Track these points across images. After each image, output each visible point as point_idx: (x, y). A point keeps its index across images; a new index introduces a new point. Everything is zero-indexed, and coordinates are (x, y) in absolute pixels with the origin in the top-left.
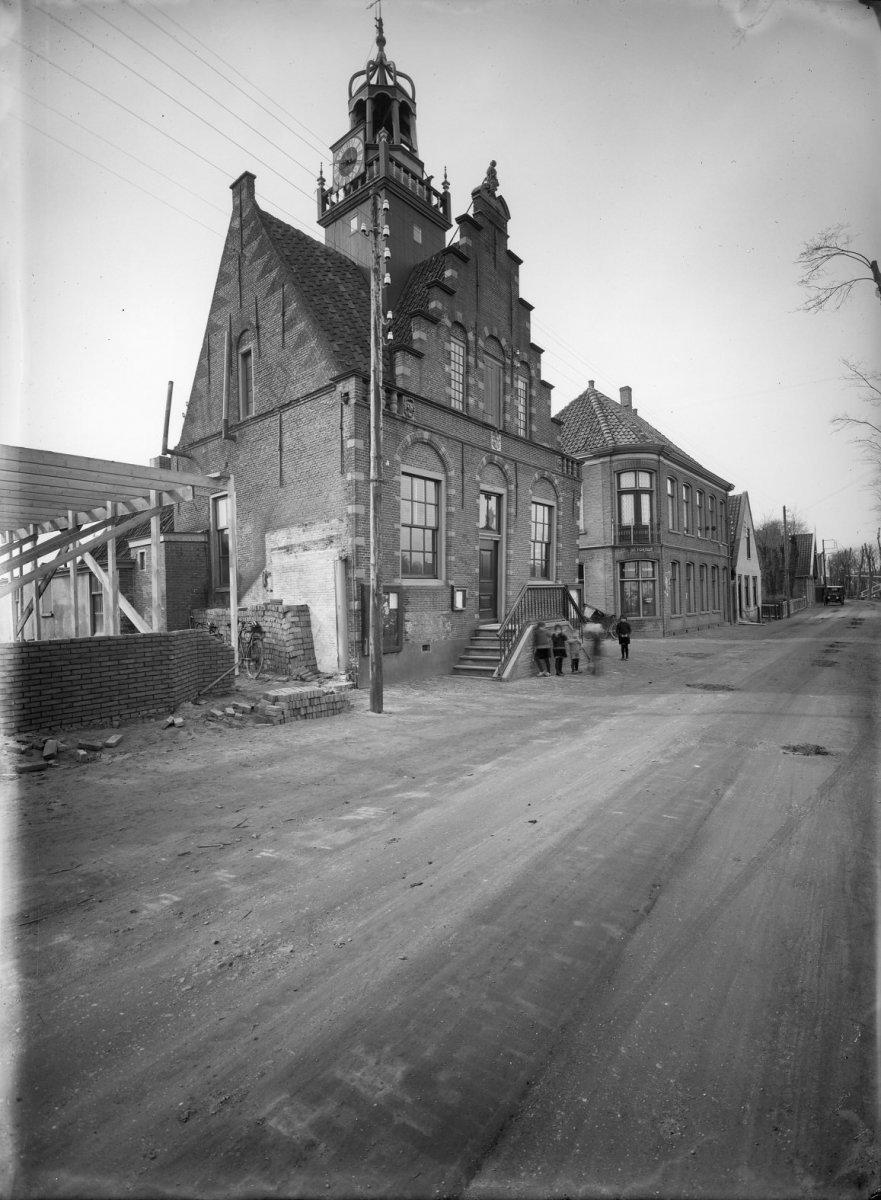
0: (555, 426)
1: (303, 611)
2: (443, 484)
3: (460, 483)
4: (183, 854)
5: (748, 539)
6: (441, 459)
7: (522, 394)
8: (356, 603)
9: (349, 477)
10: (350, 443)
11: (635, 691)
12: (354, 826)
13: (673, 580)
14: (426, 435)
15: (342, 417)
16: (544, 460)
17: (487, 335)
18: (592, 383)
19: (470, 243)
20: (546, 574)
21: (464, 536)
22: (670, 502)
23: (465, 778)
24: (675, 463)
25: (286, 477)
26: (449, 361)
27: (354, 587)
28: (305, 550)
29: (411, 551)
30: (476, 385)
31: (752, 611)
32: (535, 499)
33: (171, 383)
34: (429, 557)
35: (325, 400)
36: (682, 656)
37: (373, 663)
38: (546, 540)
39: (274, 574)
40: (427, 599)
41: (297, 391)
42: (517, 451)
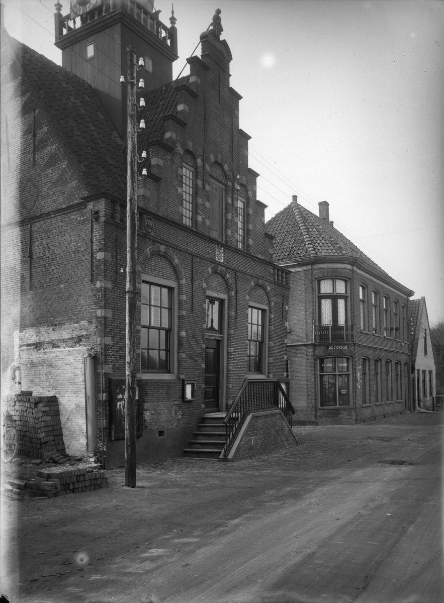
0: (267, 240)
1: (52, 402)
2: (176, 291)
5: (425, 338)
6: (175, 268)
7: (240, 212)
9: (98, 284)
10: (100, 256)
12: (153, 559)
13: (364, 374)
14: (163, 248)
15: (92, 232)
16: (259, 270)
17: (213, 160)
18: (295, 198)
20: (259, 369)
21: (193, 336)
23: (222, 529)
24: (367, 273)
27: (102, 381)
29: (148, 349)
30: (204, 205)
34: (163, 353)
35: (75, 216)
36: (373, 439)
37: (128, 446)
42: (238, 262)
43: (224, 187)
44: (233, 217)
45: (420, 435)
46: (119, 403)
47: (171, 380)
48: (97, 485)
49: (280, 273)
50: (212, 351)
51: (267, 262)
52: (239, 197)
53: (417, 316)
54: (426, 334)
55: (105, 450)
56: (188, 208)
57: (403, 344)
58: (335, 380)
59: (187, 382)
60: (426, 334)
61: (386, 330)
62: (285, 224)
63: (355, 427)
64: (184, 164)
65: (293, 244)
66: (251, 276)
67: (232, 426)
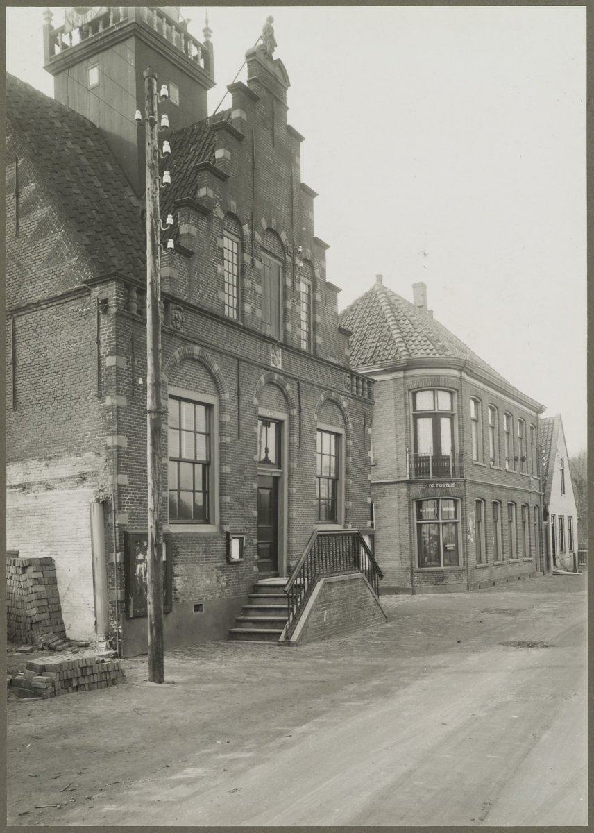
1: (47, 565)
2: (216, 409)
3: (235, 408)
4: (24, 814)
6: (214, 378)
7: (304, 298)
8: (119, 554)
9: (108, 401)
10: (110, 361)
11: (445, 650)
12: (190, 782)
13: (478, 522)
14: (197, 350)
15: (99, 329)
16: (330, 379)
17: (265, 227)
18: (380, 278)
19: (244, 117)
20: (332, 516)
21: (241, 472)
22: (474, 428)
25: (20, 398)
26: (221, 260)
27: (116, 536)
28: (48, 488)
29: (179, 491)
30: (253, 289)
31: (568, 559)
32: (320, 426)
34: (199, 496)
35: (75, 306)
37: (152, 626)
38: (333, 475)
40: (199, 549)
41: (38, 292)
42: (301, 368)
43: (280, 264)
44: (293, 306)
46: (138, 567)
47: (210, 533)
49: (360, 383)
50: (267, 492)
51: (342, 367)
54: (563, 465)
55: (120, 631)
57: (532, 480)
60: (563, 465)
61: (509, 460)
63: (467, 596)
64: (225, 233)
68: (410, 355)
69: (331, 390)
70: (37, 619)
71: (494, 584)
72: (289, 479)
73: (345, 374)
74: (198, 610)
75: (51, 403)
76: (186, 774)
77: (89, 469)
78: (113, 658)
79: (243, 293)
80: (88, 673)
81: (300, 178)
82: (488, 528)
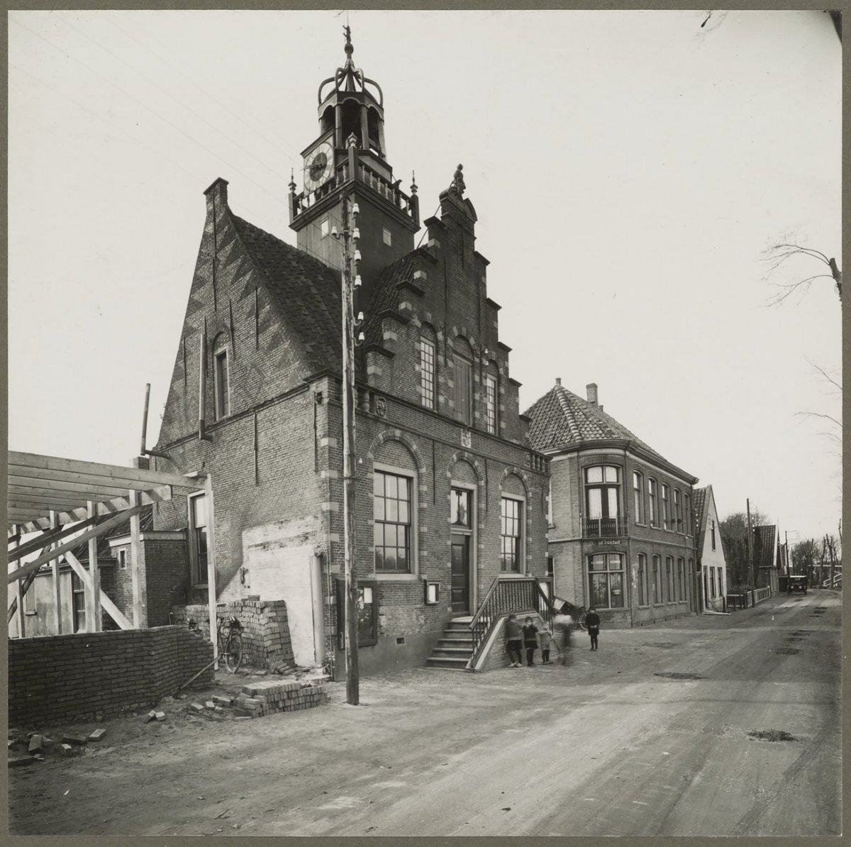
2: (415, 480)
5: (713, 531)
7: (490, 391)
8: (332, 598)
9: (324, 474)
10: (324, 442)
13: (640, 572)
14: (398, 433)
15: (315, 416)
16: (513, 457)
17: (456, 334)
18: (559, 380)
20: (516, 568)
21: (436, 532)
22: (636, 496)
25: (261, 476)
26: (419, 360)
27: (330, 583)
29: (384, 547)
30: (446, 384)
32: (505, 494)
33: (149, 385)
34: (402, 552)
35: (299, 400)
37: (348, 656)
38: (516, 534)
39: (251, 571)
40: (400, 593)
42: (487, 448)
43: (470, 364)
44: (481, 398)
45: (707, 641)
47: (411, 581)
48: (314, 702)
49: (539, 460)
50: (460, 548)
51: (522, 447)
52: (489, 376)
53: (703, 506)
54: (713, 527)
55: (334, 659)
56: (427, 387)
57: (687, 538)
58: (607, 580)
59: (430, 583)
60: (713, 527)
61: (667, 523)
62: (547, 410)
63: (631, 632)
64: (422, 338)
65: (557, 430)
66: (505, 463)
67: (480, 632)
68: (582, 439)
69: (514, 466)
70: (272, 649)
71: (654, 622)
72: (478, 537)
73: (525, 452)
74: (401, 643)
75: (282, 478)
76: (336, 803)
77: (309, 530)
78: (327, 681)
79: (438, 387)
80: (293, 696)
81: (486, 295)
82: (649, 578)
